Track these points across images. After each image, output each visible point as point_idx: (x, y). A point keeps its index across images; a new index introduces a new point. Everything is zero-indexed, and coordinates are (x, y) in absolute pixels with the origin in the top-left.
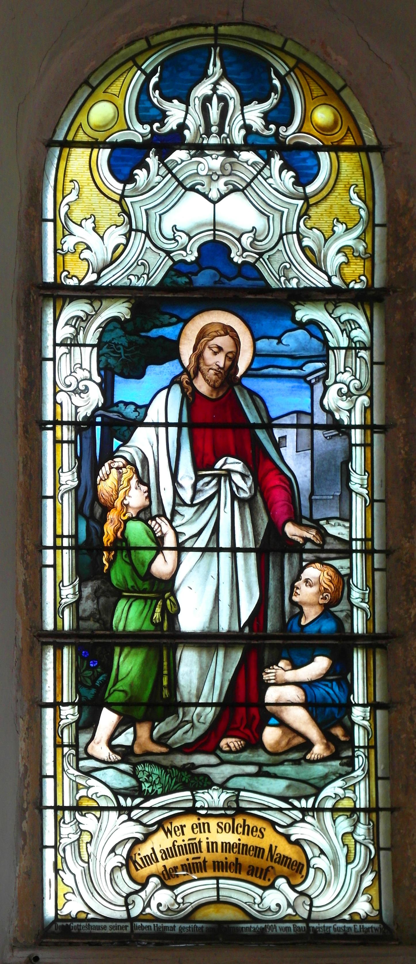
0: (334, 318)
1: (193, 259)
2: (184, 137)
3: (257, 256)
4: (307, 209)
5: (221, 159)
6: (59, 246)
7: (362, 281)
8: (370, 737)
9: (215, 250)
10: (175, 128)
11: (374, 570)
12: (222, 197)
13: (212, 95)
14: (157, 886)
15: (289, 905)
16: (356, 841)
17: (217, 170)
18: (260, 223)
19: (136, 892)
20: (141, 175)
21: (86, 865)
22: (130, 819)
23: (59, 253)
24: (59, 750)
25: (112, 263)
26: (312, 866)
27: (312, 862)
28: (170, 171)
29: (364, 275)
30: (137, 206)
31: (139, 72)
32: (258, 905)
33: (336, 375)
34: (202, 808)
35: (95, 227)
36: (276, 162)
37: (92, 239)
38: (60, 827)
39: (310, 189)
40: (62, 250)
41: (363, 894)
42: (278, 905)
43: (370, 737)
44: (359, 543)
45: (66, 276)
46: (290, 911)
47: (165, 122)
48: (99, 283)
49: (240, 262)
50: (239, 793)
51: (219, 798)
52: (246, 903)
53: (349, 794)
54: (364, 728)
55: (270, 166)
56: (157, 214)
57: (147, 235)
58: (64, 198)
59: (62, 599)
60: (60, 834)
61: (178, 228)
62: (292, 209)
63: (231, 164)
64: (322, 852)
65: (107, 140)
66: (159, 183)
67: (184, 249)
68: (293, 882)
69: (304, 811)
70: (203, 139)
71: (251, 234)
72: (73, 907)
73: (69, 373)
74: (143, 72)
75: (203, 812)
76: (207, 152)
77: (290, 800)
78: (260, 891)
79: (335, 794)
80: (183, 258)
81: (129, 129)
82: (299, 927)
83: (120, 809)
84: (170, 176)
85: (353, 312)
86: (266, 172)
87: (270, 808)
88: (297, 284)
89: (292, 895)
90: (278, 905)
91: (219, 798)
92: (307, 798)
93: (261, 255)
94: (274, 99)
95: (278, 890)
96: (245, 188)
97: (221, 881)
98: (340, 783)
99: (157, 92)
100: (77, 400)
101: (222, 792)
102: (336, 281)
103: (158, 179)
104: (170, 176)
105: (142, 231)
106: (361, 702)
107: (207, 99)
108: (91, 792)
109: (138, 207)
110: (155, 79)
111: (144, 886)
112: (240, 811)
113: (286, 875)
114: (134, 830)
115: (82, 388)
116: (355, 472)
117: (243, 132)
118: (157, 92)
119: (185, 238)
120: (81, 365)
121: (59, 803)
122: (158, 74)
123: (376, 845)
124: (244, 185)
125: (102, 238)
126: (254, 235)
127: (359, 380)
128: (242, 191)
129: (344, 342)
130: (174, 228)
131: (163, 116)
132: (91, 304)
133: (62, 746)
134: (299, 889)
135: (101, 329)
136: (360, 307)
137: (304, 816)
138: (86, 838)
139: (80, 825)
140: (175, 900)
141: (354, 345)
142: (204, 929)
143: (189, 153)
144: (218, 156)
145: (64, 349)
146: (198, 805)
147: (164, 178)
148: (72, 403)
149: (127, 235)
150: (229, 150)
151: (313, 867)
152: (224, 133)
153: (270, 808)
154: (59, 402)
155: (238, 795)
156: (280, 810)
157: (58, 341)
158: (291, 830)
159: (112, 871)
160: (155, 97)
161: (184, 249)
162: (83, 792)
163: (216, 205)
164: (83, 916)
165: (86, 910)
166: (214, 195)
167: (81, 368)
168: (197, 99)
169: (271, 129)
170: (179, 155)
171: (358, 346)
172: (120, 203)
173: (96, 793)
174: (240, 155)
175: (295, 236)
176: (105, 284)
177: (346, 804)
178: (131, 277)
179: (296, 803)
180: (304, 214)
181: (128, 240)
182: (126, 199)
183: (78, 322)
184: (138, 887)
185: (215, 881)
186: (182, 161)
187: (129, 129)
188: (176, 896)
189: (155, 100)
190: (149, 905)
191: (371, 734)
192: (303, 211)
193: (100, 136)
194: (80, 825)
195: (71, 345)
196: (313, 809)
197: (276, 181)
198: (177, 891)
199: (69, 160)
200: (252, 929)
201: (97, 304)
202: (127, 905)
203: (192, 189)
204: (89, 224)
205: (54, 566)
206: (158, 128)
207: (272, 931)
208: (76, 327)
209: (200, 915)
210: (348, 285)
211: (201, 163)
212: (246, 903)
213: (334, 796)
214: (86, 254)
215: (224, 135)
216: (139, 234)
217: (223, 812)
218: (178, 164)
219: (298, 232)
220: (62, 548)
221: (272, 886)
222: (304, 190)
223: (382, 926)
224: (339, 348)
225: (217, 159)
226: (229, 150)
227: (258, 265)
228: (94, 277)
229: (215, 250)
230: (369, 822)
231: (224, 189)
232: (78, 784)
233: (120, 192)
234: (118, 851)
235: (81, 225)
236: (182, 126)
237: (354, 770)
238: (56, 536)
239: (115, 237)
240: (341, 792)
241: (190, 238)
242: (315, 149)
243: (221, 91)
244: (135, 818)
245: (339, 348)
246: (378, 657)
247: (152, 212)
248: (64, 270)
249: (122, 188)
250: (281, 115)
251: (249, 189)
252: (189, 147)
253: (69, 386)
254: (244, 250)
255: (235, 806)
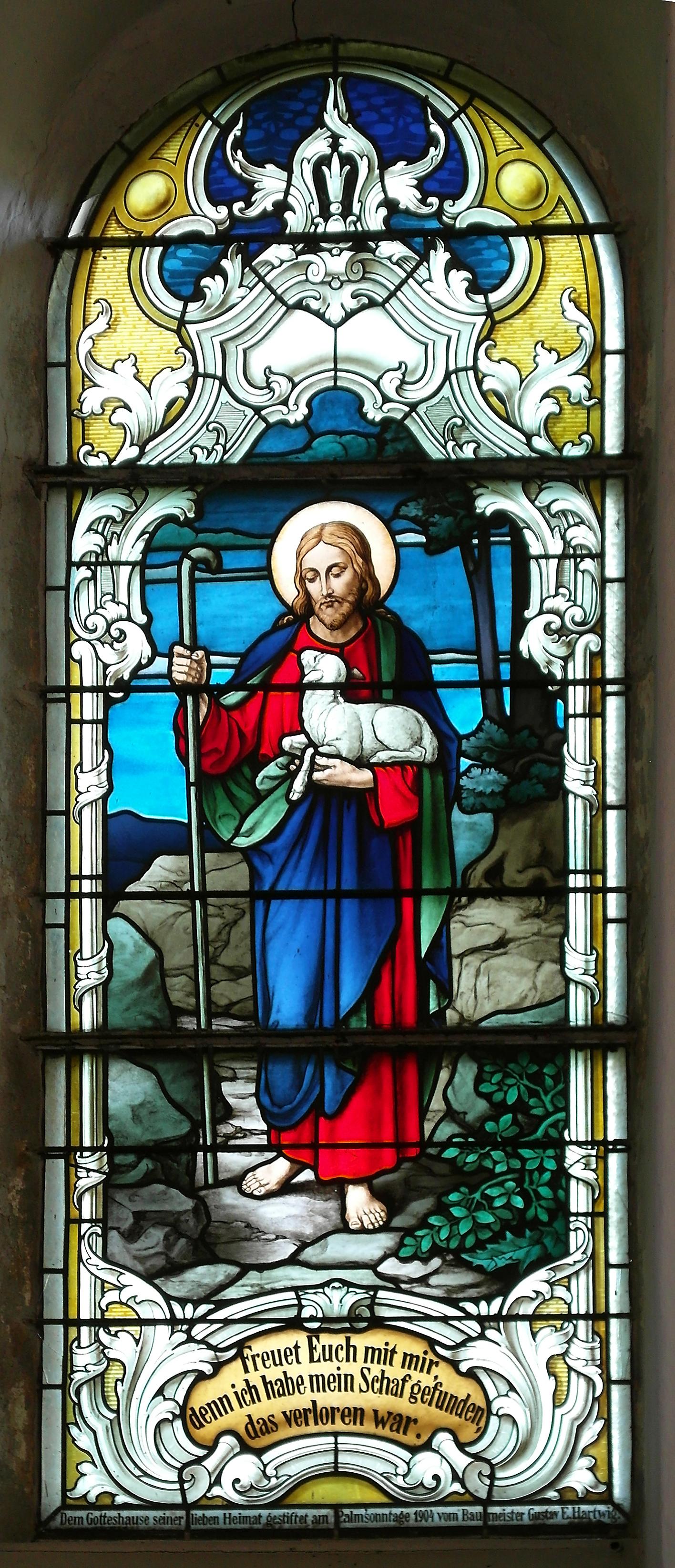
0: (539, 509)
1: (300, 418)
2: (285, 224)
3: (407, 409)
4: (490, 332)
5: (347, 255)
6: (75, 405)
7: (582, 442)
8: (596, 1197)
9: (336, 401)
10: (270, 208)
11: (606, 921)
12: (349, 315)
13: (331, 155)
14: (232, 1449)
15: (455, 1477)
16: (570, 1369)
17: (342, 274)
18: (413, 355)
19: (199, 1460)
20: (213, 286)
21: (112, 1416)
22: (190, 1339)
23: (76, 416)
24: (74, 1227)
25: (163, 429)
26: (495, 1412)
27: (494, 1407)
28: (261, 279)
29: (587, 433)
30: (205, 338)
31: (209, 123)
32: (405, 1476)
33: (542, 601)
34: (313, 1319)
35: (138, 372)
36: (440, 257)
37: (133, 393)
38: (72, 1353)
39: (495, 297)
40: (81, 411)
41: (583, 1454)
42: (436, 1477)
43: (596, 1197)
44: (580, 877)
45: (88, 453)
46: (457, 1487)
47: (253, 200)
48: (143, 462)
49: (378, 419)
50: (376, 1293)
51: (341, 1302)
52: (381, 1475)
53: (560, 1291)
54: (587, 1183)
55: (428, 263)
56: (240, 348)
57: (223, 382)
58: (85, 327)
59: (79, 980)
60: (72, 1365)
61: (273, 369)
62: (466, 331)
63: (362, 262)
64: (512, 1388)
65: (157, 235)
66: (243, 298)
67: (285, 403)
68: (463, 1439)
69: (481, 1320)
70: (317, 226)
71: (398, 374)
72: (92, 1484)
73: (92, 609)
74: (216, 123)
75: (315, 1325)
76: (323, 245)
77: (461, 1305)
78: (406, 1455)
79: (537, 1292)
80: (283, 417)
81: (195, 214)
82: (472, 1514)
83: (173, 1322)
84: (261, 285)
85: (566, 498)
86: (422, 272)
87: (428, 1318)
88: (475, 451)
89: (461, 1461)
90: (436, 1477)
91: (341, 1302)
92: (489, 1299)
93: (413, 407)
94: (435, 154)
95: (437, 1452)
96: (387, 300)
97: (341, 1439)
98: (543, 1274)
99: (239, 152)
100: (107, 654)
101: (348, 1292)
102: (541, 444)
103: (243, 291)
104: (261, 285)
105: (214, 377)
106: (582, 1138)
107: (324, 161)
108: (125, 1295)
109: (207, 338)
110: (236, 131)
111: (211, 1449)
112: (377, 1323)
113: (451, 1427)
114: (197, 1358)
115: (115, 633)
116: (574, 759)
117: (383, 212)
118: (239, 152)
119: (286, 385)
120: (114, 596)
121: (73, 1315)
122: (240, 125)
123: (604, 1376)
124: (385, 294)
125: (149, 390)
126: (404, 374)
127: (581, 606)
128: (383, 305)
129: (556, 547)
130: (269, 371)
131: (248, 191)
132: (129, 495)
133: (80, 1221)
134: (473, 1450)
135: (147, 536)
136: (581, 484)
137: (484, 1329)
138: (115, 1372)
139: (106, 1351)
140: (264, 1472)
141: (572, 551)
142: (310, 1519)
143: (294, 249)
144: (342, 250)
145: (84, 572)
146: (306, 1314)
147: (251, 289)
148: (98, 658)
149: (190, 383)
150: (360, 241)
151: (497, 1415)
152: (351, 214)
153: (428, 1318)
154: (77, 657)
155: (374, 1297)
156: (445, 1319)
157: (76, 558)
158: (463, 1353)
159: (158, 1426)
160: (237, 162)
161: (285, 403)
162: (112, 1296)
163: (338, 329)
164: (107, 1501)
165: (113, 1489)
166: (335, 314)
167: (113, 601)
168: (305, 162)
169: (431, 205)
170: (278, 252)
171: (579, 552)
172: (178, 332)
173: (135, 1297)
174: (377, 247)
175: (471, 373)
176: (153, 463)
177: (554, 1308)
178: (196, 450)
179: (470, 1307)
180: (487, 336)
181: (192, 391)
182: (187, 326)
183: (108, 525)
184: (201, 1452)
185: (331, 1439)
186: (282, 262)
187: (195, 214)
188: (265, 1466)
189: (236, 167)
190: (218, 1482)
191: (599, 1193)
192: (485, 333)
193: (147, 230)
194: (106, 1351)
195: (97, 564)
196: (498, 1317)
197: (438, 286)
198: (266, 1458)
199: (93, 280)
200: (392, 1517)
201: (139, 496)
202: (181, 1481)
203: (299, 305)
204: (126, 369)
205: (67, 926)
206: (241, 210)
207: (426, 1521)
208: (105, 534)
209: (304, 1496)
210: (560, 450)
211: (312, 263)
212: (381, 1475)
213: (533, 1295)
214: (121, 416)
215: (351, 218)
216: (209, 381)
217: (347, 1325)
218: (274, 268)
219: (475, 368)
220: (81, 895)
221: (427, 1446)
222: (486, 298)
223: (611, 1509)
224: (547, 557)
225: (339, 255)
226: (360, 241)
227: (407, 422)
228: (134, 452)
229: (336, 401)
230: (593, 1338)
231: (352, 304)
232: (103, 1282)
233: (178, 315)
234: (168, 1393)
235: (113, 370)
236: (282, 206)
237: (567, 1254)
238: (69, 878)
239: (171, 387)
240: (545, 1288)
241: (294, 386)
242: (505, 233)
243: (346, 147)
244: (199, 1338)
245: (547, 557)
246: (610, 1063)
247: (231, 347)
248: (84, 444)
249: (181, 309)
250: (447, 181)
251: (393, 301)
252: (293, 239)
253: (95, 631)
254: (386, 399)
255: (367, 1314)
